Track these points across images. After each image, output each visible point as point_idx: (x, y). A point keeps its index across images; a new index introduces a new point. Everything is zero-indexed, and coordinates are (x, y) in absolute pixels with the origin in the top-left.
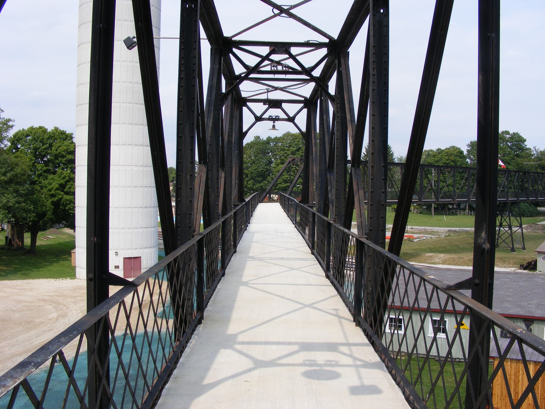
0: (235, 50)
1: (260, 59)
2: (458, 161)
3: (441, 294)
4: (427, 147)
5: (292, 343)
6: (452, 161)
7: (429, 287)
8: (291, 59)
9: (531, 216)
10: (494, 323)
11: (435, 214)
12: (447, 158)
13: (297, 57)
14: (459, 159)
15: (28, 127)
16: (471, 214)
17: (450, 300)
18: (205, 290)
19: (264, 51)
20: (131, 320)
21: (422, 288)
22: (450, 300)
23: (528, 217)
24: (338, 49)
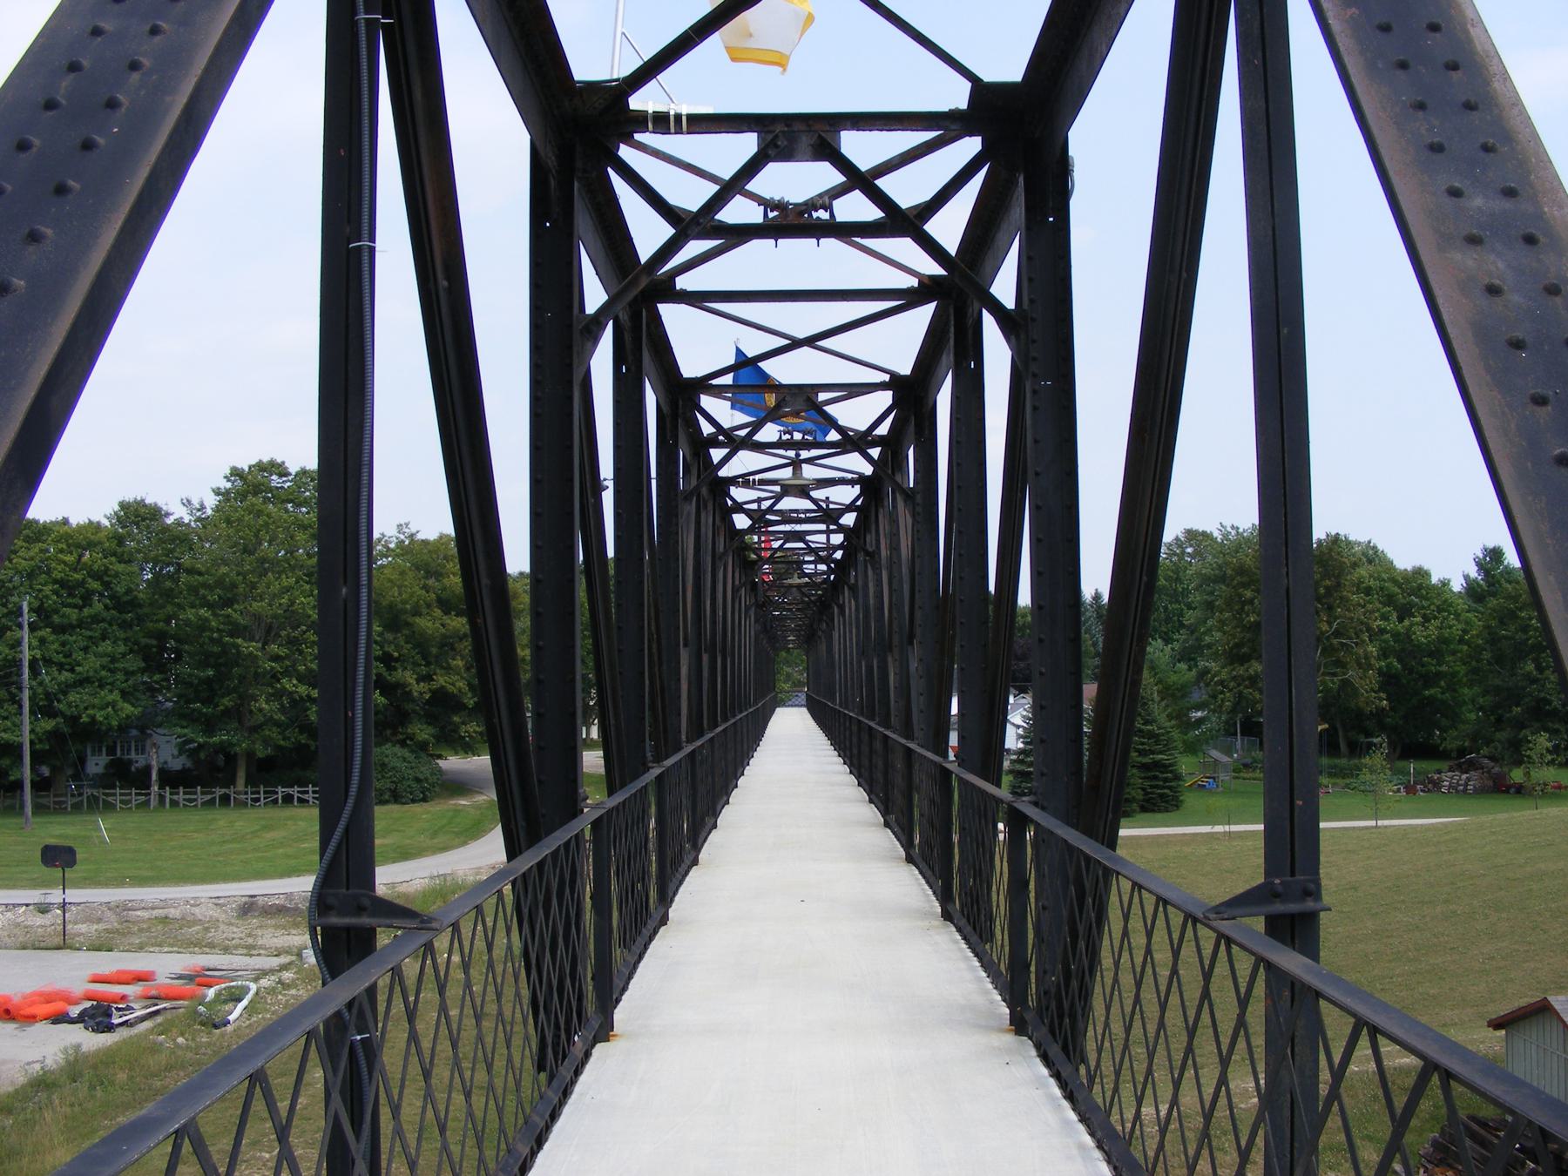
0: (625, 152)
1: (713, 188)
2: (117, 575)
3: (1203, 931)
4: (1172, 530)
5: (1340, 980)
6: (97, 576)
7: (1177, 919)
8: (857, 193)
9: (424, 800)
10: (1318, 994)
11: (39, 809)
12: (69, 558)
13: (880, 183)
14: (120, 567)
15: (1357, 533)
16: (174, 804)
17: (1223, 947)
18: (617, 952)
19: (729, 153)
20: (420, 1026)
21: (1161, 922)
22: (1223, 947)
23: (413, 801)
24: (1021, 131)
